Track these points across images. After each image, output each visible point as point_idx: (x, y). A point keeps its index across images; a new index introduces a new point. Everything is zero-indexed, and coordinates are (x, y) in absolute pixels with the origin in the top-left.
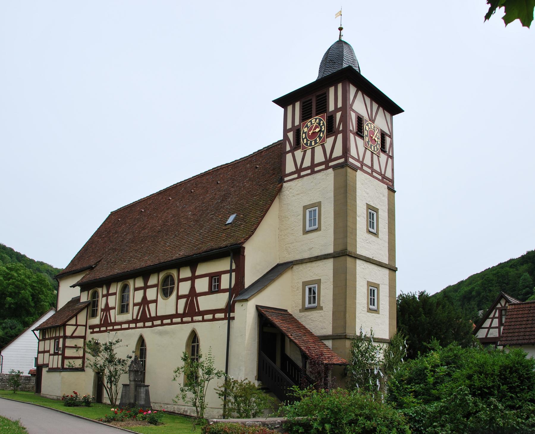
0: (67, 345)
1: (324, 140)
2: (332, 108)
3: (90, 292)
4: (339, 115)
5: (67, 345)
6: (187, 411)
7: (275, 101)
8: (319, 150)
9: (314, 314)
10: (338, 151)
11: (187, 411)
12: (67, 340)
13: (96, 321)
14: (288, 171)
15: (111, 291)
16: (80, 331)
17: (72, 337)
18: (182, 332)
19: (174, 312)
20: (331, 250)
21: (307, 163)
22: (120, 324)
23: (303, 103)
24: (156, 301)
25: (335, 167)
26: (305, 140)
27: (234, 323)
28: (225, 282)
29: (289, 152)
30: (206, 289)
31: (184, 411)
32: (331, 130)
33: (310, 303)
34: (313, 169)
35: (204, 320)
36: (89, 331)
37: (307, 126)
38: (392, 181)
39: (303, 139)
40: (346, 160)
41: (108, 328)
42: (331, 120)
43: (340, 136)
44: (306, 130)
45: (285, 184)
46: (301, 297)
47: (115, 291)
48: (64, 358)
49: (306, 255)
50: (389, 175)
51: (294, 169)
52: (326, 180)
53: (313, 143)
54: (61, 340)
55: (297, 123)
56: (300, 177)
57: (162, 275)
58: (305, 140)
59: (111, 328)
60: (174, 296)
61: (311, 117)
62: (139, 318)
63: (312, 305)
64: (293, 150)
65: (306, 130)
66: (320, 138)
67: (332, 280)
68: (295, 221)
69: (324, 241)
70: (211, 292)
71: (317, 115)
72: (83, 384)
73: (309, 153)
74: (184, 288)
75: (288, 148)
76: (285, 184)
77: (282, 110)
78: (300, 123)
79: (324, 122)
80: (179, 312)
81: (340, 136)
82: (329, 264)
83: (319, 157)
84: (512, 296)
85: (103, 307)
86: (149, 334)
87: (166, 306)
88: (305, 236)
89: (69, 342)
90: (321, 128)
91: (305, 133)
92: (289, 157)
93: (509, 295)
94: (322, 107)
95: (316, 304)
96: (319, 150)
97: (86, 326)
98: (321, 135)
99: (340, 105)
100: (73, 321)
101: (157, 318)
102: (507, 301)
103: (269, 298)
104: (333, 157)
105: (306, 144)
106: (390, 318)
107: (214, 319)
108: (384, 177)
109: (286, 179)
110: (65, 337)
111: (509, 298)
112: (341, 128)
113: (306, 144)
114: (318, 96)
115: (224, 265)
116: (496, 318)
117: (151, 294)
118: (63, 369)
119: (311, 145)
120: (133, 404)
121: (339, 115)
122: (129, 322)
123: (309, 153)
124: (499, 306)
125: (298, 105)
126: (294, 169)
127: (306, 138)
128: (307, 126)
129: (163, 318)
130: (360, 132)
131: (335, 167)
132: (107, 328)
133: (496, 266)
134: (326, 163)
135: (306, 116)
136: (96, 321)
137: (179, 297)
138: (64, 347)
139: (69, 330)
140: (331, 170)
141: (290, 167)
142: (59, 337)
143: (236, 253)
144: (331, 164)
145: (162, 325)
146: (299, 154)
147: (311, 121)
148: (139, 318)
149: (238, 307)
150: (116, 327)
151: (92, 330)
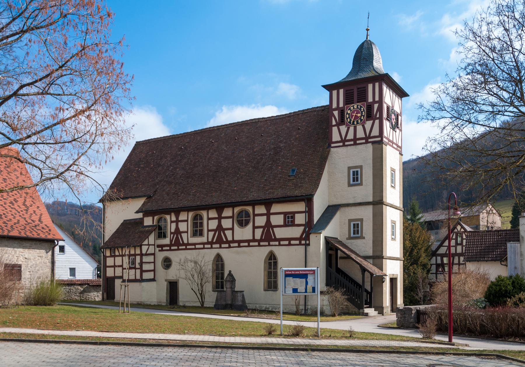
0: (143, 261)
1: (364, 122)
2: (370, 100)
3: (156, 218)
4: (376, 106)
5: (143, 261)
6: (268, 308)
7: (324, 87)
8: (360, 128)
9: (359, 242)
10: (375, 132)
11: (268, 308)
12: (143, 257)
13: (167, 241)
14: (334, 140)
15: (180, 218)
16: (151, 250)
17: (146, 255)
18: (263, 252)
19: (251, 238)
20: (371, 199)
21: (350, 136)
22: (194, 244)
23: (346, 91)
24: (232, 229)
25: (373, 143)
26: (349, 119)
27: (309, 248)
28: (300, 219)
29: (334, 126)
30: (282, 223)
31: (266, 308)
32: (370, 116)
33: (354, 234)
34: (355, 141)
35: (280, 245)
36: (157, 249)
37: (350, 109)
38: (401, 148)
39: (347, 119)
40: (382, 140)
41: (180, 247)
42: (370, 108)
43: (377, 122)
44: (349, 112)
45: (332, 149)
46: (347, 230)
47: (186, 219)
48: (142, 271)
49: (351, 201)
50: (400, 145)
51: (339, 139)
52: (366, 151)
53: (355, 123)
54: (138, 258)
55: (341, 105)
56: (344, 145)
57: (237, 210)
58: (349, 119)
59: (184, 247)
60: (250, 225)
61: (353, 103)
62: (214, 241)
63: (356, 235)
64: (338, 125)
65: (349, 112)
66: (361, 120)
67: (372, 220)
68: (343, 178)
69: (365, 192)
70: (285, 225)
71: (358, 102)
72: (155, 292)
73: (352, 129)
74: (261, 221)
75: (334, 123)
76: (332, 149)
77: (328, 93)
78: (344, 105)
79: (364, 108)
80: (256, 238)
81: (377, 122)
82: (370, 208)
83: (360, 134)
84: (468, 225)
85: (173, 230)
86: (226, 254)
87: (244, 233)
88: (350, 188)
89: (145, 259)
90: (362, 113)
91: (349, 114)
92: (335, 130)
93: (464, 223)
94: (363, 97)
95: (360, 235)
96: (360, 128)
97: (154, 245)
98: (362, 118)
99: (377, 99)
100: (146, 242)
101: (234, 241)
102: (462, 227)
103: (330, 231)
104: (371, 135)
105: (350, 122)
106: (400, 243)
107: (290, 244)
108: (398, 146)
109: (333, 145)
110: (141, 255)
111: (464, 225)
112: (378, 116)
113: (350, 122)
114: (358, 88)
115: (301, 206)
116: (454, 239)
117: (226, 223)
118: (142, 280)
119: (353, 124)
120: (230, 304)
121: (376, 106)
122: (204, 244)
123: (352, 129)
124: (456, 230)
125: (341, 91)
126: (339, 139)
127: (349, 117)
128: (350, 109)
129: (239, 242)
130: (388, 118)
131: (373, 143)
132: (178, 247)
133: (268, 105)
134: (367, 139)
135: (348, 100)
136: (167, 241)
137: (254, 228)
138: (141, 263)
139: (144, 249)
140: (370, 145)
141: (336, 137)
142: (135, 255)
143: (309, 200)
144: (369, 140)
145: (239, 246)
146: (343, 129)
147: (353, 106)
148: (214, 241)
149: (312, 237)
150: (188, 247)
151: (160, 249)
